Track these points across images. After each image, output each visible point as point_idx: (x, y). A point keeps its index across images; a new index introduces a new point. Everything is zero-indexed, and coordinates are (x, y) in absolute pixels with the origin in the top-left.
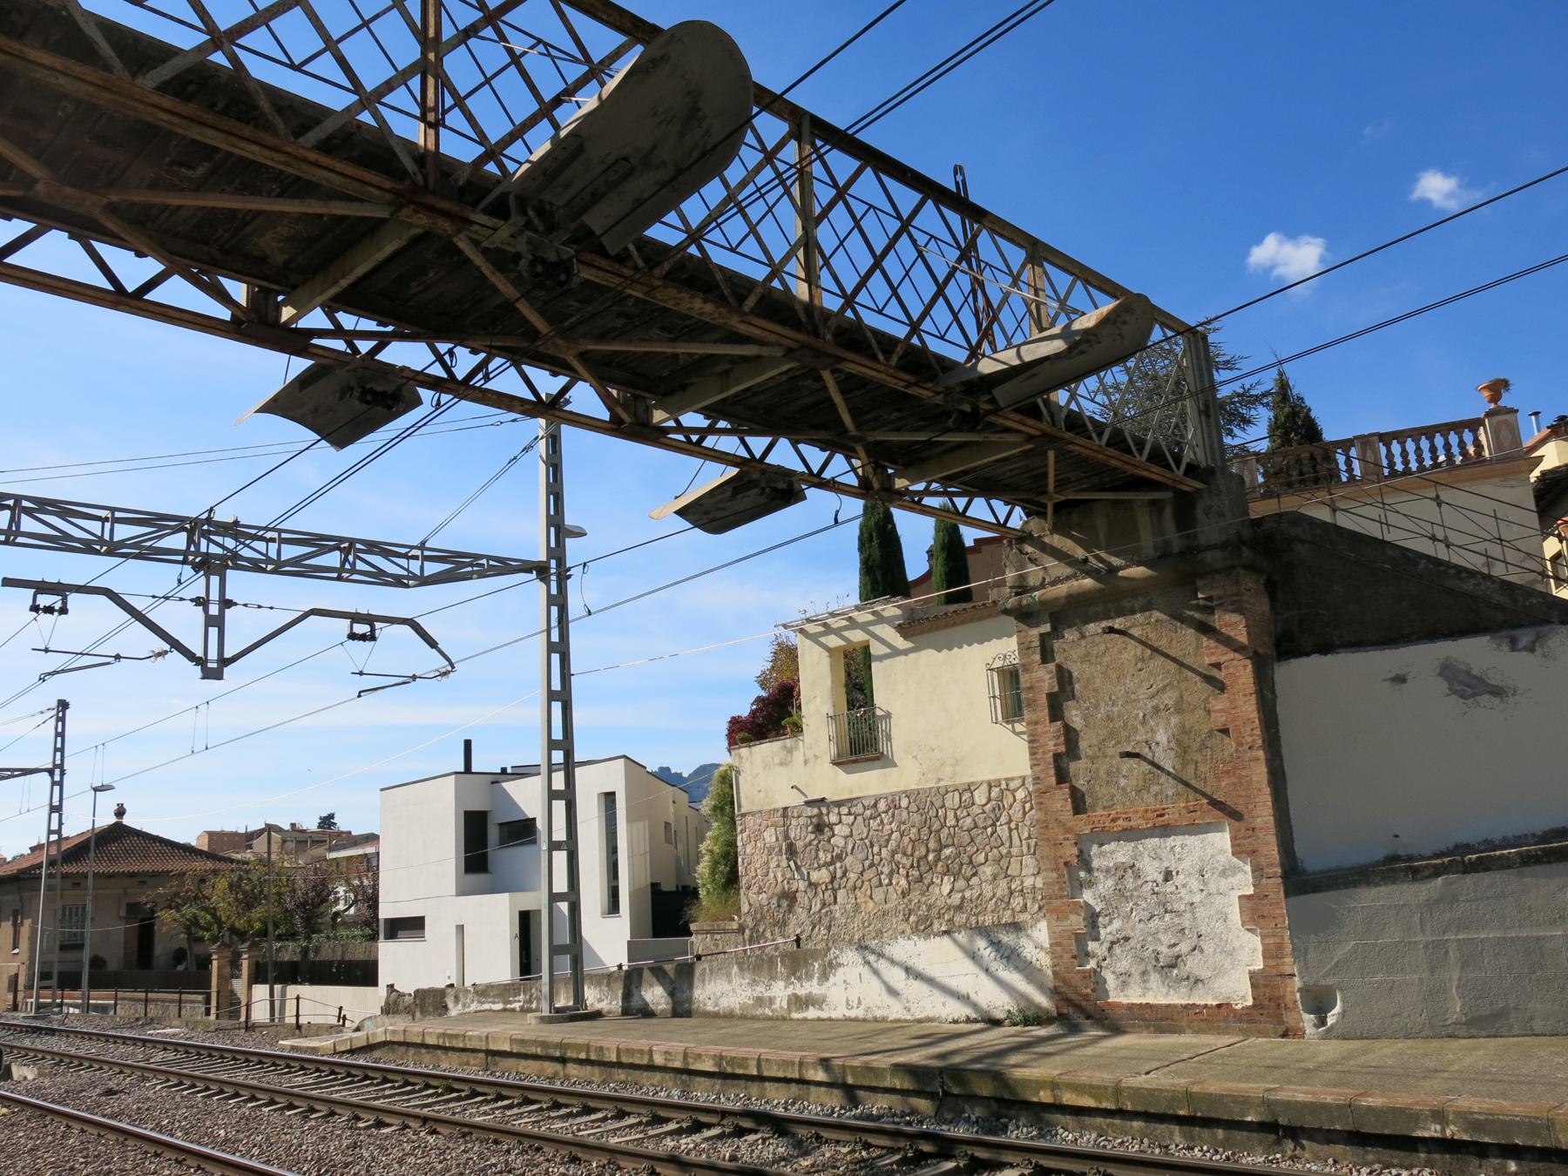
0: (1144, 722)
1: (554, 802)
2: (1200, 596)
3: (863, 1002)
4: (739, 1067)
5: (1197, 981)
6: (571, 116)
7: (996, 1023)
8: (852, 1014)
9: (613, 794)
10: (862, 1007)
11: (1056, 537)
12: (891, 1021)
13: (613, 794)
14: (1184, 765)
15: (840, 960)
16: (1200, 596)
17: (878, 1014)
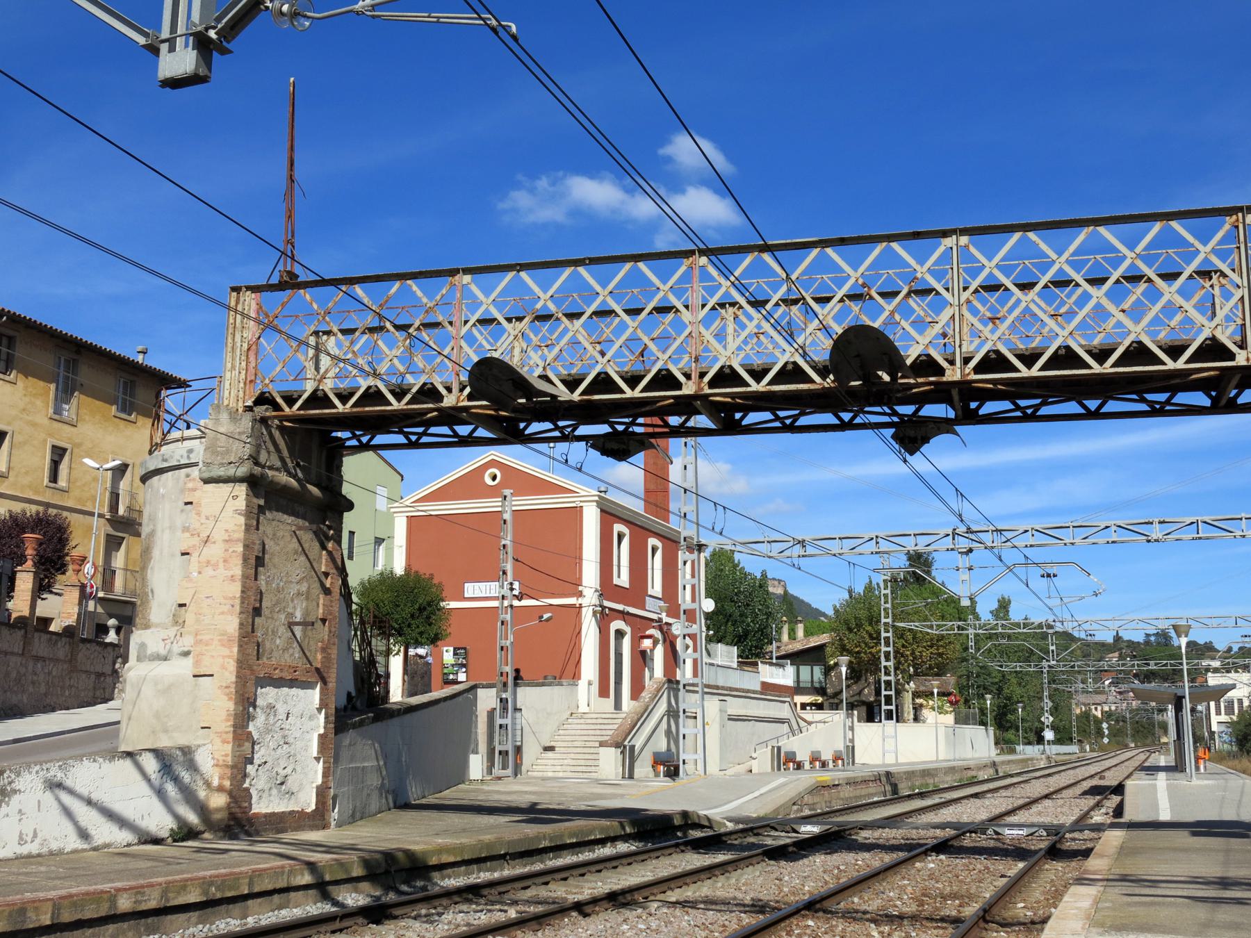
0: (292, 601)
1: (466, 595)
2: (327, 523)
3: (40, 835)
4: (230, 890)
5: (293, 793)
6: (800, 286)
7: (157, 841)
8: (24, 850)
9: (1217, 714)
10: (38, 841)
11: (278, 432)
12: (67, 853)
13: (1217, 714)
14: (305, 638)
15: (15, 786)
16: (327, 523)
17: (54, 846)
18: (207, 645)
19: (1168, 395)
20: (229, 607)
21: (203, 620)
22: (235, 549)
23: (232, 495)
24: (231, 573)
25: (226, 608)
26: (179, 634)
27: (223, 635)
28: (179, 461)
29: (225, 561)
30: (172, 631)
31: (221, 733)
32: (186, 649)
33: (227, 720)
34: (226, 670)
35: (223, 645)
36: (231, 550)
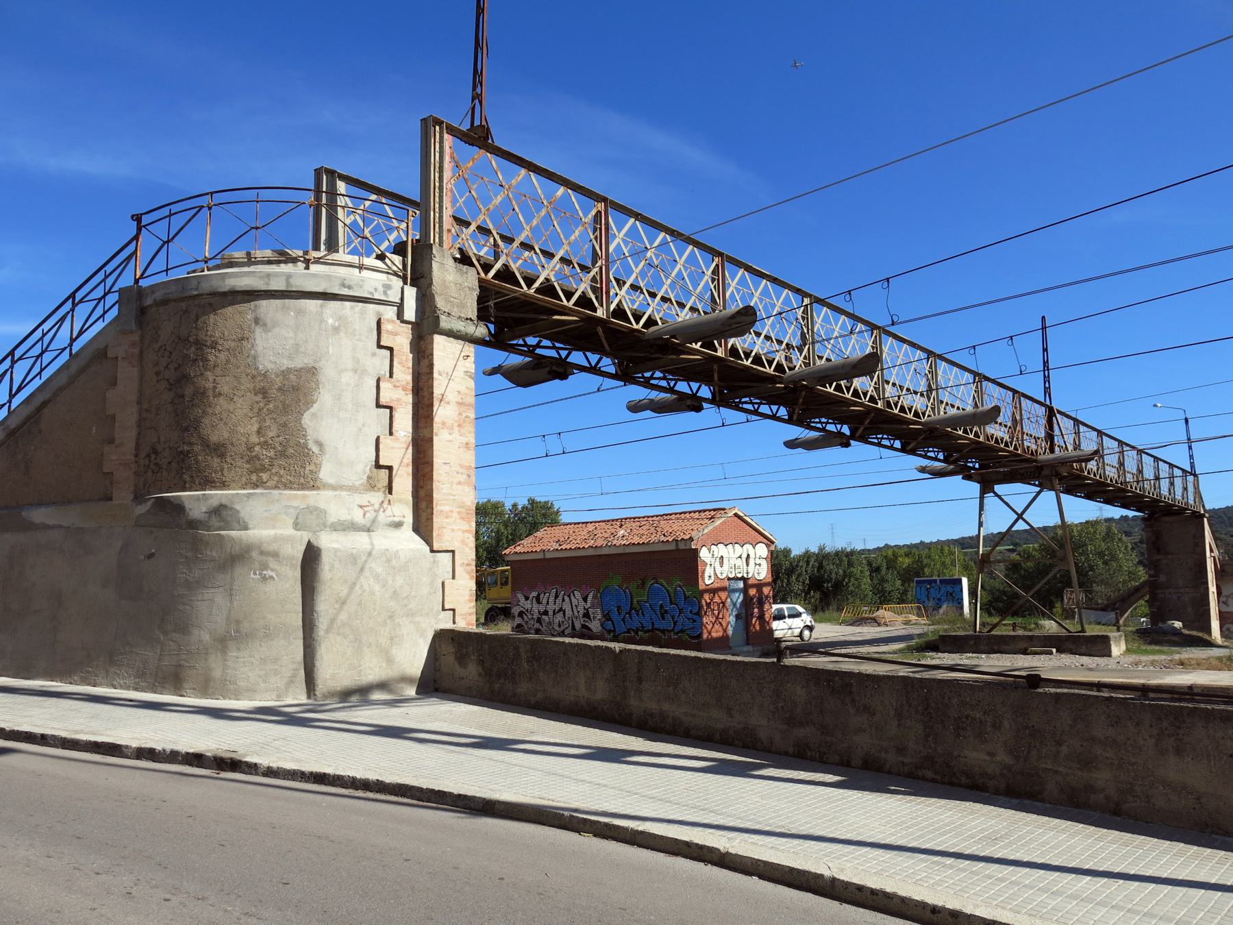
18: (447, 517)
19: (651, 373)
20: (465, 476)
21: (442, 489)
22: (469, 415)
23: (463, 354)
24: (465, 440)
25: (463, 478)
26: (386, 502)
27: (462, 507)
28: (371, 293)
29: (459, 426)
30: (376, 497)
31: (465, 615)
32: (397, 519)
33: (470, 601)
34: (467, 545)
35: (463, 519)
36: (464, 415)
